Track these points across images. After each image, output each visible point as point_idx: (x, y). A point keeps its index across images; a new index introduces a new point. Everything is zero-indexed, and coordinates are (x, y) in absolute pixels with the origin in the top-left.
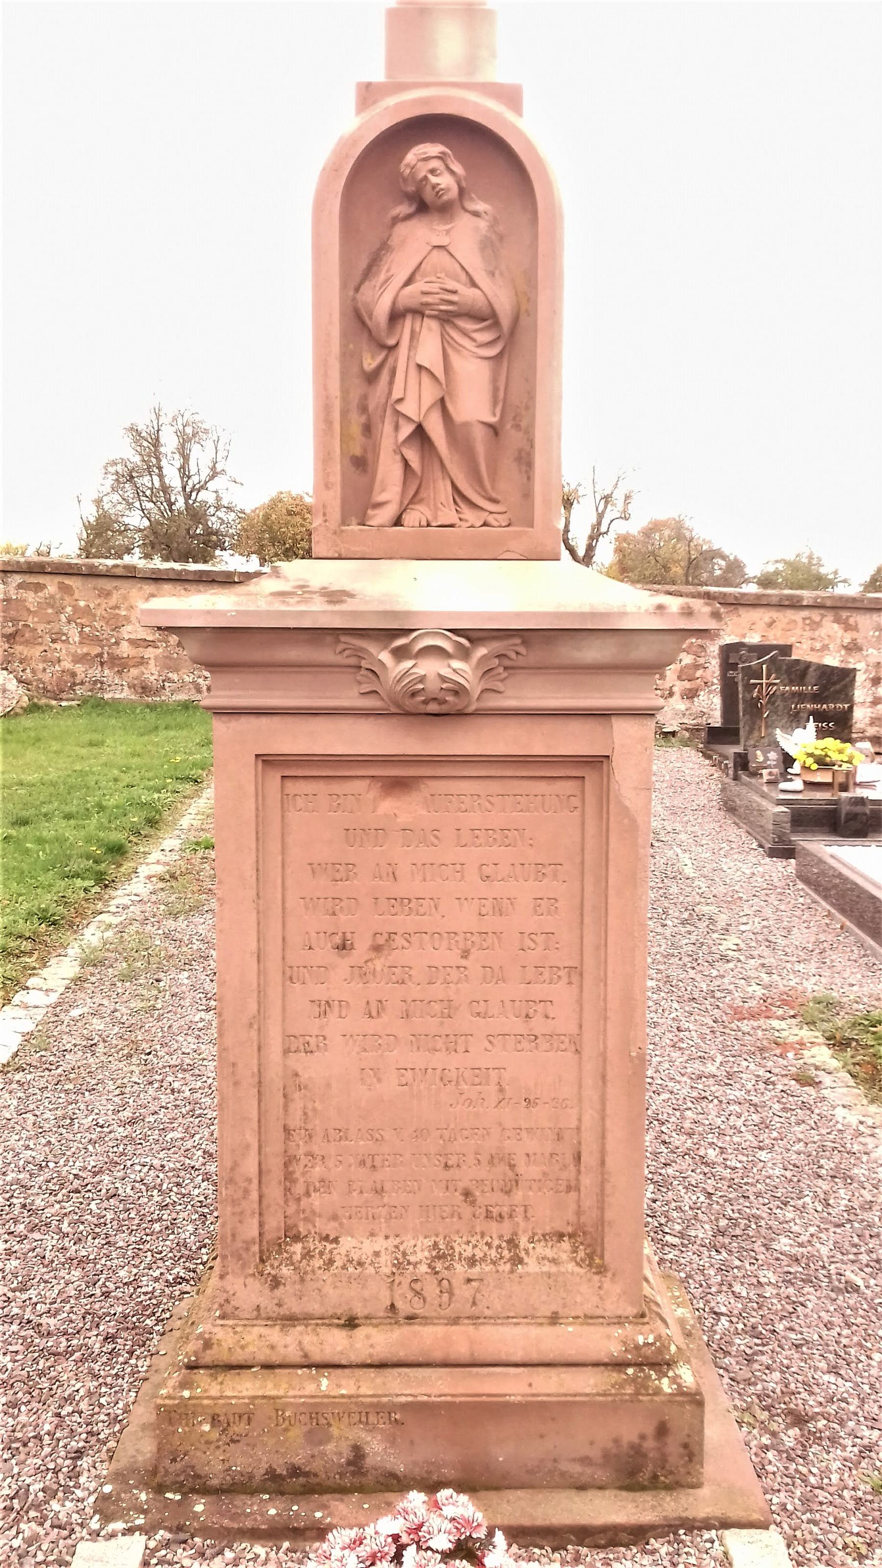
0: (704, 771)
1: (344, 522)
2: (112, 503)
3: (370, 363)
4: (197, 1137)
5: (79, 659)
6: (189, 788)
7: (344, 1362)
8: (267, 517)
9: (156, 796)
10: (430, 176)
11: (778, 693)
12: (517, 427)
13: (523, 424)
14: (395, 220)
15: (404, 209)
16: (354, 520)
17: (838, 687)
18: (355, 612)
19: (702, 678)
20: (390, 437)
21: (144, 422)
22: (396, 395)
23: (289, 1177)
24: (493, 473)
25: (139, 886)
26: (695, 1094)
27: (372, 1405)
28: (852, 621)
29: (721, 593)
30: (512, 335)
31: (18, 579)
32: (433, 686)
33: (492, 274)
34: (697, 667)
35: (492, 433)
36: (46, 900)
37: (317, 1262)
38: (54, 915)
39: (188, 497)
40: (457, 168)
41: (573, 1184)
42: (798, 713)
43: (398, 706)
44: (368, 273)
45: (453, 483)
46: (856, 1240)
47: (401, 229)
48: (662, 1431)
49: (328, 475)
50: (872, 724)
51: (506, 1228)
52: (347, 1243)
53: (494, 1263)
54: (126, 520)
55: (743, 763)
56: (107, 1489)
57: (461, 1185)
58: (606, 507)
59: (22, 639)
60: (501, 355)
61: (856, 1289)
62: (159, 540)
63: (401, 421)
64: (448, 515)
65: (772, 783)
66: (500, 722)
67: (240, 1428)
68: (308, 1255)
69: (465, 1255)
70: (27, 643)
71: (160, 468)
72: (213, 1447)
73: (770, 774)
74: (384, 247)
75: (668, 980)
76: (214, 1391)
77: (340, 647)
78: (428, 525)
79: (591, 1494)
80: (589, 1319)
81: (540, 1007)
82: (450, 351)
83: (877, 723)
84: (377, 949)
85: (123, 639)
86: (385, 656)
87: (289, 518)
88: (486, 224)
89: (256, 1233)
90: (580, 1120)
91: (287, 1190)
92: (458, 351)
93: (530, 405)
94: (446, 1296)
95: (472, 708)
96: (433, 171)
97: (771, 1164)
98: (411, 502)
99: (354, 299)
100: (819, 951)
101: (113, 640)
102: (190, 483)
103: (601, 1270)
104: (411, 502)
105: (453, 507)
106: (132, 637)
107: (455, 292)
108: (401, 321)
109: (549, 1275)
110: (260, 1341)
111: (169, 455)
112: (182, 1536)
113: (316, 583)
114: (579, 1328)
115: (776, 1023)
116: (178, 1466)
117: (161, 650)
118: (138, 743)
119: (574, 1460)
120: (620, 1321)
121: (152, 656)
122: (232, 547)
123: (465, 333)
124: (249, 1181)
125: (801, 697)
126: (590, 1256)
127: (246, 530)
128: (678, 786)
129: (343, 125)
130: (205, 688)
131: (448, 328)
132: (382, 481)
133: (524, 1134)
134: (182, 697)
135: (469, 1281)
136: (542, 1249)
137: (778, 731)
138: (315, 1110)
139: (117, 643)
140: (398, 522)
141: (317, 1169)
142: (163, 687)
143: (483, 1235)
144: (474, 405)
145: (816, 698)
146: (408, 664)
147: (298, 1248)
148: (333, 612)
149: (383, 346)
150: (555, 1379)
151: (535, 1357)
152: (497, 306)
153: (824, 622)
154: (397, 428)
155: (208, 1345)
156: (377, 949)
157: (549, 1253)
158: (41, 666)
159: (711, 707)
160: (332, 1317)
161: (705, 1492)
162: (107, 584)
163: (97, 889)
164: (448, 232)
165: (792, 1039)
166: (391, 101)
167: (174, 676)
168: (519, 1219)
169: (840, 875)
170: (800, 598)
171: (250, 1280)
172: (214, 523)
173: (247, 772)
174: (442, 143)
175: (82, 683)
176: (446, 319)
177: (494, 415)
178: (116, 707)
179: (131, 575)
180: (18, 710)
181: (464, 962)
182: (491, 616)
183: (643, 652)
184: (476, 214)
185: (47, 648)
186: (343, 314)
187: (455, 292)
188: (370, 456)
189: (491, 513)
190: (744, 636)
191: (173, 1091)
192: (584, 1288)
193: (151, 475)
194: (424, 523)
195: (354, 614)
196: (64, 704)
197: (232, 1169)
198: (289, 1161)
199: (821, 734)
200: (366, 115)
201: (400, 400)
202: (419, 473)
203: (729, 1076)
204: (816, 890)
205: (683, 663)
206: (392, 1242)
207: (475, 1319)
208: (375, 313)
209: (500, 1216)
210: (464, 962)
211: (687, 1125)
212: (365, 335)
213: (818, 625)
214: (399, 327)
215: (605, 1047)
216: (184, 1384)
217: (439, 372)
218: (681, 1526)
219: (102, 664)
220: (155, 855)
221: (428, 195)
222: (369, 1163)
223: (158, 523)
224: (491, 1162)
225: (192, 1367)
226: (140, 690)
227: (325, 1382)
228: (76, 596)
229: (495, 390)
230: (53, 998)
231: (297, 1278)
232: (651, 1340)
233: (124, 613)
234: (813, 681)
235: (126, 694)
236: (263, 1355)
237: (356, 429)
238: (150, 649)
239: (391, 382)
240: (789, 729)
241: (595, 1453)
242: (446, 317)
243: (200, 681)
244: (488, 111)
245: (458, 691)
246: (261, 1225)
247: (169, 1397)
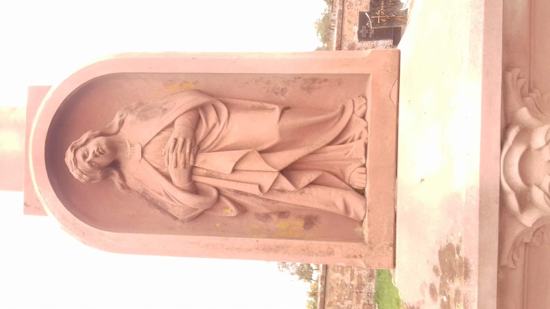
1: (360, 239)
2: (293, 270)
3: (231, 211)
5: (358, 302)
10: (88, 160)
12: (283, 91)
13: (281, 86)
14: (125, 186)
15: (116, 178)
16: (358, 229)
18: (480, 250)
20: (291, 197)
22: (257, 191)
24: (321, 111)
30: (211, 97)
33: (165, 110)
35: (287, 112)
44: (163, 210)
45: (331, 143)
47: (130, 182)
49: (321, 252)
60: (227, 104)
63: (278, 187)
74: (144, 195)
78: (364, 166)
82: (221, 146)
86: (528, 219)
88: (129, 116)
92: (223, 138)
98: (343, 180)
104: (343, 180)
105: (348, 145)
106: (349, 279)
107: (176, 140)
108: (198, 185)
123: (209, 132)
129: (53, 224)
131: (205, 146)
132: (327, 205)
137: (401, 10)
139: (352, 286)
140: (361, 192)
144: (264, 126)
148: (480, 274)
149: (218, 200)
152: (190, 106)
154: (282, 191)
170: (340, 10)
174: (67, 149)
175: (368, 301)
177: (273, 109)
184: (121, 123)
186: (194, 232)
187: (176, 140)
188: (304, 213)
189: (353, 112)
190: (354, 33)
194: (363, 170)
201: (260, 188)
202: (320, 173)
208: (192, 206)
212: (211, 213)
214: (205, 187)
217: (239, 154)
219: (360, 292)
221: (103, 160)
226: (371, 278)
229: (254, 108)
235: (373, 284)
238: (355, 273)
239: (246, 194)
242: (196, 148)
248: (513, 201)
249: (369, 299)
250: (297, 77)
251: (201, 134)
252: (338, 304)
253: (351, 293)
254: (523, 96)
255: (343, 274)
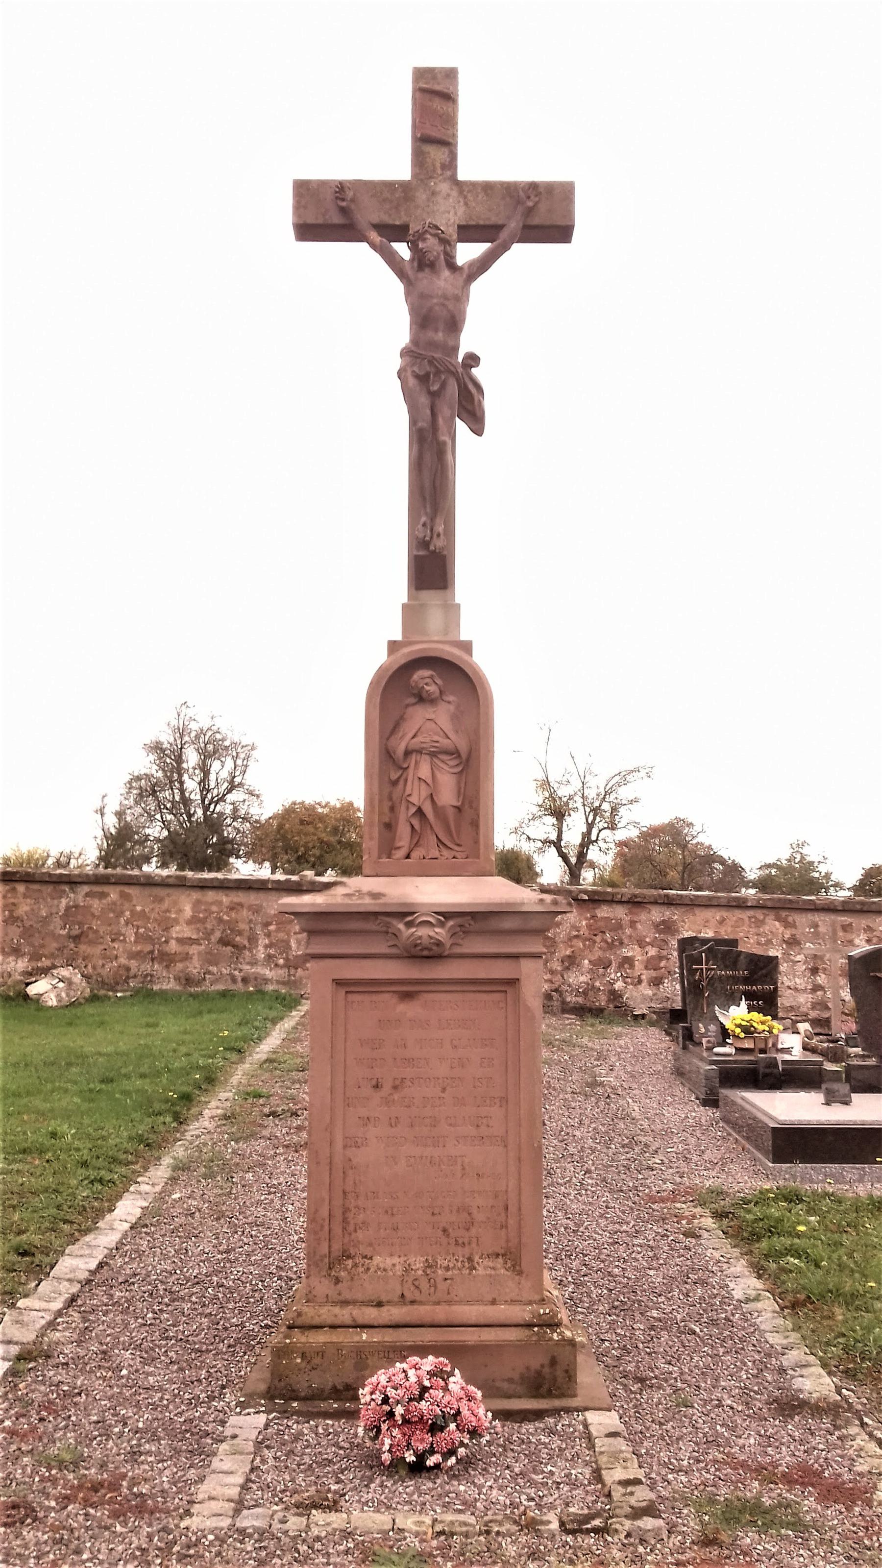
0: (663, 1045)
3: (394, 776)
4: (271, 1259)
5: (133, 956)
6: (234, 1056)
7: (376, 1324)
8: (280, 827)
9: (211, 1061)
11: (715, 977)
12: (471, 807)
14: (407, 706)
15: (412, 700)
16: (384, 856)
17: (764, 971)
19: (665, 967)
21: (167, 738)
22: (407, 793)
23: (345, 1220)
25: (206, 1123)
26: (610, 1241)
27: (391, 1347)
28: (790, 919)
29: (678, 895)
31: (86, 889)
32: (426, 941)
34: (660, 958)
36: (141, 1129)
37: (361, 1269)
38: (147, 1139)
39: (206, 809)
40: (439, 681)
41: (504, 1223)
42: (733, 993)
43: (407, 951)
44: (394, 731)
46: (701, 1312)
47: (410, 710)
48: (553, 1362)
50: (813, 1008)
51: (467, 1251)
52: (377, 1260)
53: (459, 1269)
54: (148, 831)
55: (689, 1036)
56: (242, 1399)
57: (442, 1225)
58: (594, 819)
59: (86, 940)
60: (462, 771)
61: (694, 1333)
62: (177, 849)
63: (410, 806)
64: (436, 854)
65: (709, 1049)
66: (461, 961)
67: (317, 1360)
68: (355, 1265)
69: (443, 1265)
70: (91, 943)
71: (182, 783)
72: (302, 1372)
73: (708, 1042)
75: (604, 1180)
76: (303, 1339)
77: (379, 921)
79: (512, 1400)
80: (513, 1302)
81: (484, 1121)
83: (818, 1007)
84: (395, 1088)
85: (172, 938)
86: (401, 926)
87: (301, 827)
89: (327, 1251)
90: (507, 1186)
91: (344, 1228)
93: (477, 798)
94: (433, 1289)
95: (446, 953)
96: (426, 684)
97: (656, 1277)
99: (386, 745)
100: (723, 1162)
101: (163, 939)
102: (209, 796)
103: (520, 1273)
106: (180, 936)
107: (437, 742)
109: (490, 1276)
110: (327, 1313)
111: (191, 771)
112: (286, 1415)
113: (365, 889)
114: (507, 1307)
115: (678, 1205)
116: (282, 1384)
117: (203, 947)
118: (189, 1023)
119: (504, 1380)
120: (530, 1303)
121: (195, 952)
122: (248, 855)
124: (324, 1220)
125: (735, 980)
126: (514, 1266)
127: (260, 839)
128: (640, 1055)
130: (239, 979)
133: (476, 1195)
134: (220, 987)
135: (446, 1279)
136: (487, 1262)
138: (360, 1181)
139: (167, 942)
140: (408, 857)
141: (361, 1216)
142: (204, 979)
143: (453, 1254)
145: (746, 981)
146: (414, 930)
147: (350, 1263)
149: (401, 768)
150: (493, 1334)
151: (482, 1321)
153: (767, 920)
154: (408, 808)
155: (299, 1314)
156: (395, 1088)
157: (491, 1264)
158: (100, 963)
159: (673, 990)
160: (369, 1301)
161: (579, 1399)
162: (161, 892)
163: (174, 1124)
164: (434, 712)
165: (687, 1213)
166: (406, 650)
167: (214, 969)
168: (474, 1245)
169: (755, 1118)
171: (323, 1279)
172: (229, 832)
173: (328, 988)
174: (432, 669)
175: (135, 976)
176: (433, 755)
178: (164, 996)
179: (149, 882)
180: (82, 1001)
181: (443, 1095)
182: (454, 905)
183: (535, 924)
184: (449, 702)
185: (106, 947)
187: (437, 742)
188: (393, 824)
191: (252, 1236)
192: (510, 1284)
193: (172, 789)
195: (385, 904)
196: (119, 995)
197: (315, 1213)
198: (346, 1210)
199: (750, 1009)
200: (393, 657)
201: (410, 795)
203: (637, 1232)
204: (733, 1128)
205: (649, 955)
206: (403, 1259)
207: (449, 1303)
209: (463, 1243)
210: (443, 1095)
211: (603, 1257)
213: (763, 922)
215: (520, 1141)
216: (286, 1337)
218: (562, 1410)
219: (153, 960)
220: (213, 1104)
221: (424, 695)
222: (390, 1212)
223: (177, 833)
224: (458, 1211)
225: (290, 1327)
226: (184, 982)
227: (364, 1337)
228: (134, 902)
230: (158, 1189)
231: (349, 1278)
232: (547, 1311)
233: (173, 916)
234: (744, 967)
236: (330, 1320)
237: (386, 810)
240: (725, 1007)
241: (516, 1376)
243: (236, 973)
244: (452, 654)
245: (439, 944)
246: (330, 1247)
247: (279, 1343)
248: (409, 918)
249: (139, 979)
250: (478, 815)
251: (440, 756)
252: (128, 913)
253: (149, 939)
254: (460, 926)
255: (189, 922)
